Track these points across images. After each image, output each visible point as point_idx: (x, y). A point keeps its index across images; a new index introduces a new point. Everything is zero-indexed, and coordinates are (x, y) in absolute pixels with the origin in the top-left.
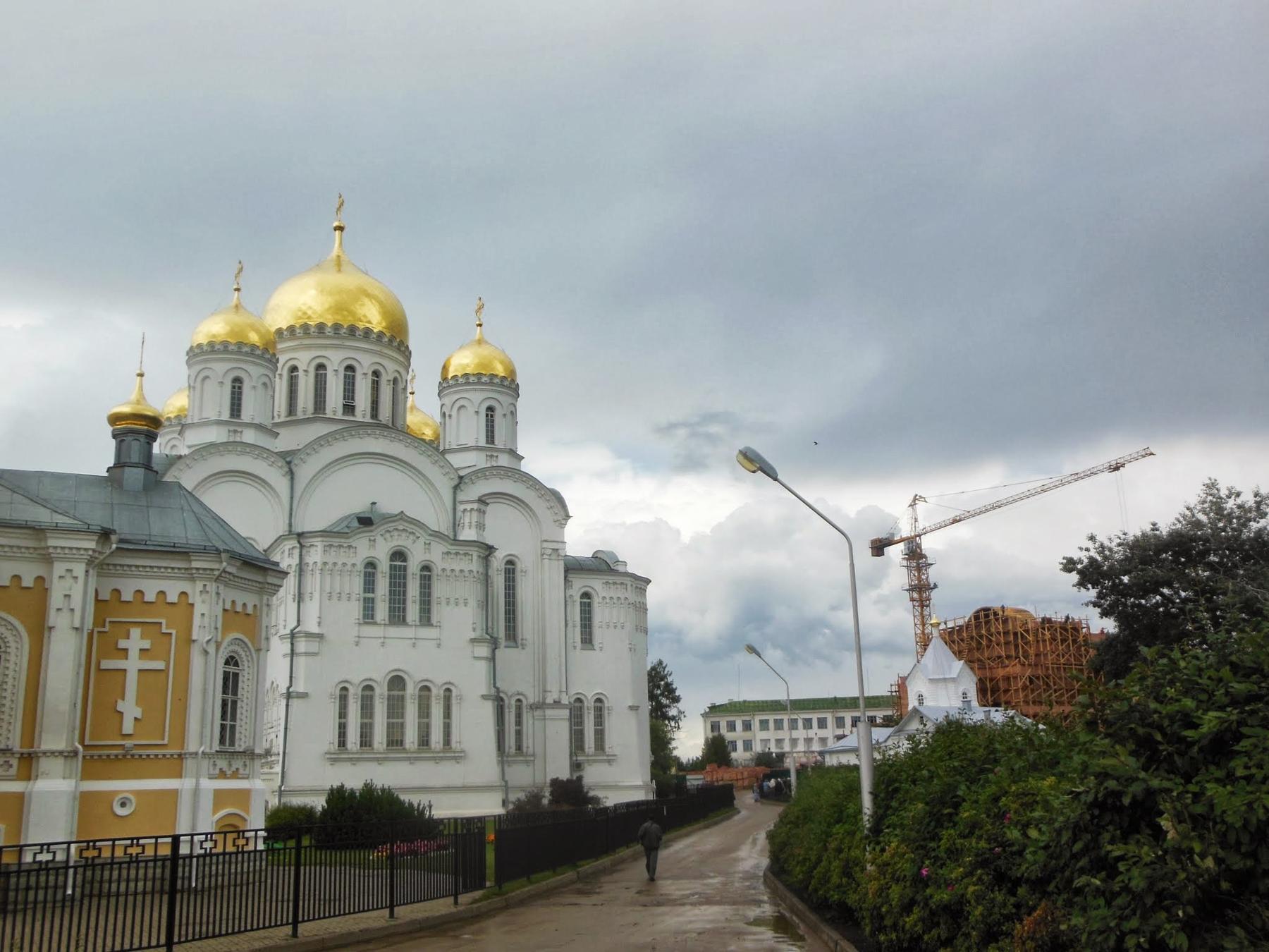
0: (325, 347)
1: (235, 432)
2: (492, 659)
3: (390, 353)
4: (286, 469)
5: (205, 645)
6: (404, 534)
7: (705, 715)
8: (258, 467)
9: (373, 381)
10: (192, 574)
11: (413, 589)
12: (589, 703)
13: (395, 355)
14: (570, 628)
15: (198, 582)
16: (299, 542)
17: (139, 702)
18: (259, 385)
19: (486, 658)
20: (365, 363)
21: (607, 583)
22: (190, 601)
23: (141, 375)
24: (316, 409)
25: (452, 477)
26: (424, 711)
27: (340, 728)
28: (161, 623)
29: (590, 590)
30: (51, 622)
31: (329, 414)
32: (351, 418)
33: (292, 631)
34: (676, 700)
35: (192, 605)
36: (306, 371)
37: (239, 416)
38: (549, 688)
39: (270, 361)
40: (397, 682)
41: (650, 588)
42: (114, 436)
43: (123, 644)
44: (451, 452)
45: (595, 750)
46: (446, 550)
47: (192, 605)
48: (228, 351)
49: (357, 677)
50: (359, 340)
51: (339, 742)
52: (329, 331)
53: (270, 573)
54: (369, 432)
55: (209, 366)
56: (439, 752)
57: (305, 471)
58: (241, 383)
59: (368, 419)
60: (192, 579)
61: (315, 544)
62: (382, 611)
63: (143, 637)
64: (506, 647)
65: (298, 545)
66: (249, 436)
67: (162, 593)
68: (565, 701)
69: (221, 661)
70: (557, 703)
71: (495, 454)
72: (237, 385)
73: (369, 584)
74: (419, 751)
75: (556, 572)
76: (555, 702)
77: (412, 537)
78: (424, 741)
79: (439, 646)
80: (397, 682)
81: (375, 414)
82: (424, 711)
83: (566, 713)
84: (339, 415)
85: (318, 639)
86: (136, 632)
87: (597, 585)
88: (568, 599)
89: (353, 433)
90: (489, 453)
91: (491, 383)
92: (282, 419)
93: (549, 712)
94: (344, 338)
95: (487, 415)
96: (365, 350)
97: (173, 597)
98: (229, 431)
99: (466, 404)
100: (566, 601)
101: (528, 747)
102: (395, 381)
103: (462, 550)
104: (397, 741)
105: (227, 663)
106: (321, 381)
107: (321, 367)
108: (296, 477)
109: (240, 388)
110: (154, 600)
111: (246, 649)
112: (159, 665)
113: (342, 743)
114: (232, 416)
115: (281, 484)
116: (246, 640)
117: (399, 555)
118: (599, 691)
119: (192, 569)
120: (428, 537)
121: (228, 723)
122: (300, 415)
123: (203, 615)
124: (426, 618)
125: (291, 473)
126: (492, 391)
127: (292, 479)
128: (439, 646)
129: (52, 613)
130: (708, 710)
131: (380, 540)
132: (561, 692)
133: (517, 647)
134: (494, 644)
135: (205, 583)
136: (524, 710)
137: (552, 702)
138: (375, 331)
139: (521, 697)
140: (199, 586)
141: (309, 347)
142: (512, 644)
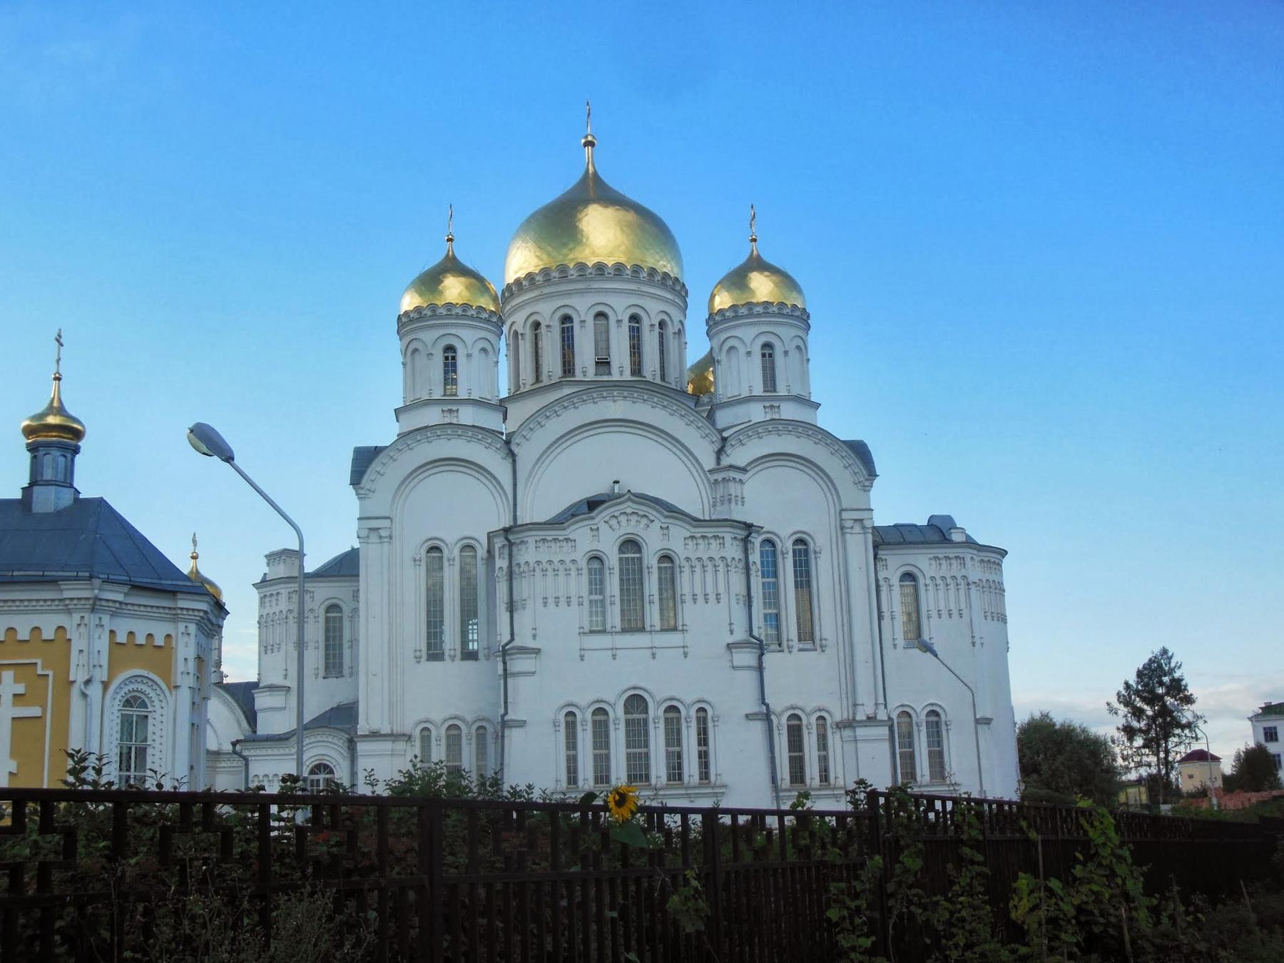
0: (569, 293)
1: (450, 411)
2: (760, 669)
3: (652, 290)
4: (507, 451)
5: (83, 687)
6: (634, 518)
7: (1255, 718)
9: (632, 329)
10: (67, 605)
11: (652, 585)
12: (921, 717)
13: (659, 292)
14: (886, 622)
15: (74, 615)
16: (507, 539)
18: (475, 352)
19: (515, 675)
20: (620, 307)
21: (936, 558)
22: (68, 637)
23: (58, 379)
24: (565, 372)
25: (714, 439)
26: (674, 736)
27: (700, 757)
28: (36, 664)
29: (915, 571)
31: (579, 376)
32: (606, 378)
33: (504, 647)
34: (1189, 700)
35: (70, 640)
36: (548, 326)
38: (860, 701)
40: (636, 702)
41: (1006, 562)
42: (32, 448)
44: (723, 407)
45: (791, 783)
46: (688, 534)
47: (70, 640)
48: (436, 315)
49: (584, 699)
50: (610, 280)
51: (569, 778)
52: (574, 274)
53: (180, 596)
54: (605, 394)
55: (453, 331)
56: (695, 787)
57: (527, 452)
58: (455, 352)
59: (627, 376)
60: (69, 612)
61: (525, 539)
62: (614, 617)
63: (16, 681)
64: (800, 650)
65: (507, 543)
66: (467, 416)
67: (36, 629)
68: (882, 715)
69: (117, 704)
70: (871, 720)
71: (776, 404)
72: (450, 355)
73: (597, 584)
74: (700, 786)
75: (859, 547)
76: (869, 718)
77: (644, 521)
79: (686, 655)
80: (636, 702)
81: (637, 369)
82: (674, 736)
83: (885, 731)
84: (591, 376)
85: (534, 655)
87: (923, 561)
88: (882, 583)
89: (585, 398)
90: (767, 404)
91: (766, 314)
92: (528, 388)
93: (861, 732)
94: (591, 280)
95: (764, 355)
96: (615, 291)
97: (48, 633)
98: (443, 411)
99: (736, 345)
100: (878, 586)
101: (782, 780)
102: (662, 324)
104: (641, 776)
105: (128, 703)
106: (568, 337)
107: (567, 319)
108: (518, 459)
109: (454, 358)
110: (52, 638)
111: (154, 687)
112: (35, 711)
114: (633, 373)
115: (501, 469)
116: (152, 676)
117: (631, 544)
118: (933, 701)
119: (64, 599)
120: (664, 520)
122: (546, 381)
123: (81, 651)
125: (512, 455)
126: (769, 323)
127: (514, 462)
128: (686, 655)
130: (1260, 711)
131: (604, 528)
132: (876, 704)
133: (782, 651)
134: (761, 649)
135: (82, 614)
137: (864, 718)
138: (590, 265)
139: (824, 714)
140: (76, 617)
142: (809, 646)
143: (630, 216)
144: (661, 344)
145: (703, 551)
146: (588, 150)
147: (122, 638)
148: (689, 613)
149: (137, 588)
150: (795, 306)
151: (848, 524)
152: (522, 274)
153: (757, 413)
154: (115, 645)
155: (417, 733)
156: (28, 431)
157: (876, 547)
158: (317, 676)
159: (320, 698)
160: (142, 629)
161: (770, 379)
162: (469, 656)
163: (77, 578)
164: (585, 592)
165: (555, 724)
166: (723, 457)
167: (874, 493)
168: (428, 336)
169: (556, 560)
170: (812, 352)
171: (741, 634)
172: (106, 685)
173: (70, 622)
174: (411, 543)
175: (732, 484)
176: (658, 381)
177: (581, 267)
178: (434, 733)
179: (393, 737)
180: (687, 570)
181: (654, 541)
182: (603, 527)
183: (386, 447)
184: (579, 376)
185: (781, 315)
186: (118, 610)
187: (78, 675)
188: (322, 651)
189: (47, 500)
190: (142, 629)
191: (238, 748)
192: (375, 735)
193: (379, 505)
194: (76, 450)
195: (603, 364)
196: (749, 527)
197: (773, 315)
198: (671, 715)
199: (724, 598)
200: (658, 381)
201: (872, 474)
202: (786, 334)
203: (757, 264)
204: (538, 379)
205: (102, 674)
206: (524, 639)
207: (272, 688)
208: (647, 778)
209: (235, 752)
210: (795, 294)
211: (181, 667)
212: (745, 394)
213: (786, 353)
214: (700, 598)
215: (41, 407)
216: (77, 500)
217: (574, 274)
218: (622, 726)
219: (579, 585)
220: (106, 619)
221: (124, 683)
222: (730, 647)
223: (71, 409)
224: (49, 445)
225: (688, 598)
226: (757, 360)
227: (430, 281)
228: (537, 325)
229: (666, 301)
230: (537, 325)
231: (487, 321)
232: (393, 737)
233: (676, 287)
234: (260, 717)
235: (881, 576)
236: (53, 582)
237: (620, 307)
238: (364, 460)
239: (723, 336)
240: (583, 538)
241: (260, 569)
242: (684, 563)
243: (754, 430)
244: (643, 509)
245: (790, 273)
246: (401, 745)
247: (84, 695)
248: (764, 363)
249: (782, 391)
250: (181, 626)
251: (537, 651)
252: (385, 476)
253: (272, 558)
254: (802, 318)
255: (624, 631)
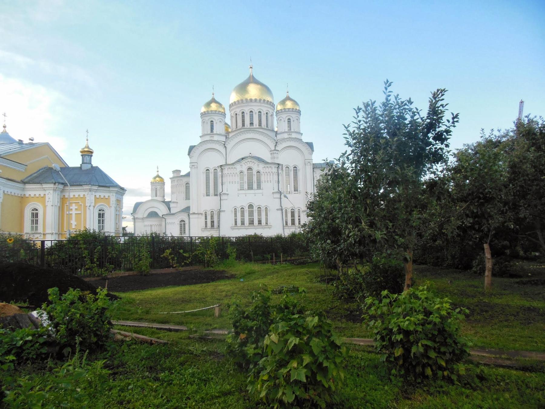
6: (251, 163)
8: (217, 146)
9: (259, 115)
17: (76, 221)
18: (218, 122)
19: (222, 200)
20: (256, 110)
30: (46, 205)
32: (252, 127)
37: (213, 132)
39: (224, 115)
40: (251, 206)
42: (82, 156)
43: (71, 208)
49: (239, 206)
52: (245, 101)
57: (229, 146)
59: (258, 126)
62: (246, 186)
63: (76, 206)
66: (216, 138)
73: (242, 179)
74: (266, 226)
75: (309, 169)
78: (260, 222)
80: (251, 206)
86: (74, 205)
88: (315, 177)
92: (240, 128)
103: (269, 166)
107: (243, 113)
113: (206, 226)
114: (259, 126)
117: (250, 169)
121: (34, 225)
122: (238, 128)
124: (259, 187)
129: (46, 202)
136: (301, 213)
141: (239, 107)
143: (259, 86)
144: (267, 118)
145: (267, 170)
146: (251, 69)
147: (98, 197)
148: (263, 185)
149: (99, 186)
150: (296, 109)
151: (307, 163)
152: (233, 102)
153: (286, 136)
154: (96, 198)
155: (204, 213)
156: (81, 152)
157: (313, 169)
158: (204, 196)
159: (183, 205)
160: (102, 195)
161: (290, 127)
162: (216, 195)
163: (86, 185)
164: (239, 180)
165: (232, 211)
166: (276, 147)
167: (313, 155)
168: (207, 118)
169: (232, 173)
170: (301, 121)
171: (276, 190)
172: (94, 207)
173: (86, 193)
174: (202, 169)
175: (275, 154)
176: (266, 128)
177: (246, 100)
178: (208, 213)
179: (198, 214)
180: (263, 175)
181: (255, 168)
182: (243, 164)
183: (195, 146)
184: (246, 127)
185: (293, 111)
186: (96, 191)
187: (88, 205)
188: (185, 194)
189: (86, 167)
190: (102, 195)
191: (164, 216)
192: (194, 213)
193: (195, 159)
194: (91, 156)
195: (252, 124)
196: (279, 164)
197: (291, 111)
198: (242, 210)
199: (272, 182)
200: (266, 128)
201: (313, 150)
202: (293, 116)
203: (288, 98)
204: (237, 127)
205: (93, 204)
206: (225, 192)
207: (174, 202)
208: (253, 224)
209: (163, 217)
210: (296, 106)
211: (111, 202)
212: (283, 131)
213: (294, 121)
214: (269, 182)
215: (84, 147)
216: (92, 167)
217: (245, 101)
218: (248, 212)
219: (237, 179)
220: (93, 193)
221: (98, 207)
222: (273, 193)
223: (91, 147)
224: (85, 155)
225: (264, 182)
226: (287, 122)
227: (208, 104)
228: (236, 114)
229: (268, 107)
230: (236, 114)
231: (221, 114)
232: (198, 214)
233: (272, 105)
234: (172, 209)
235: (315, 175)
236: (81, 185)
237: (256, 110)
238: (191, 148)
239: (279, 116)
240: (238, 167)
241: (172, 175)
242: (262, 173)
243: (284, 140)
244: (253, 160)
245: (296, 100)
246: (200, 216)
247: (89, 209)
248: (288, 124)
249: (292, 130)
250: (112, 194)
251: (228, 194)
252: (196, 153)
253: (174, 172)
254: (299, 112)
255: (248, 189)
